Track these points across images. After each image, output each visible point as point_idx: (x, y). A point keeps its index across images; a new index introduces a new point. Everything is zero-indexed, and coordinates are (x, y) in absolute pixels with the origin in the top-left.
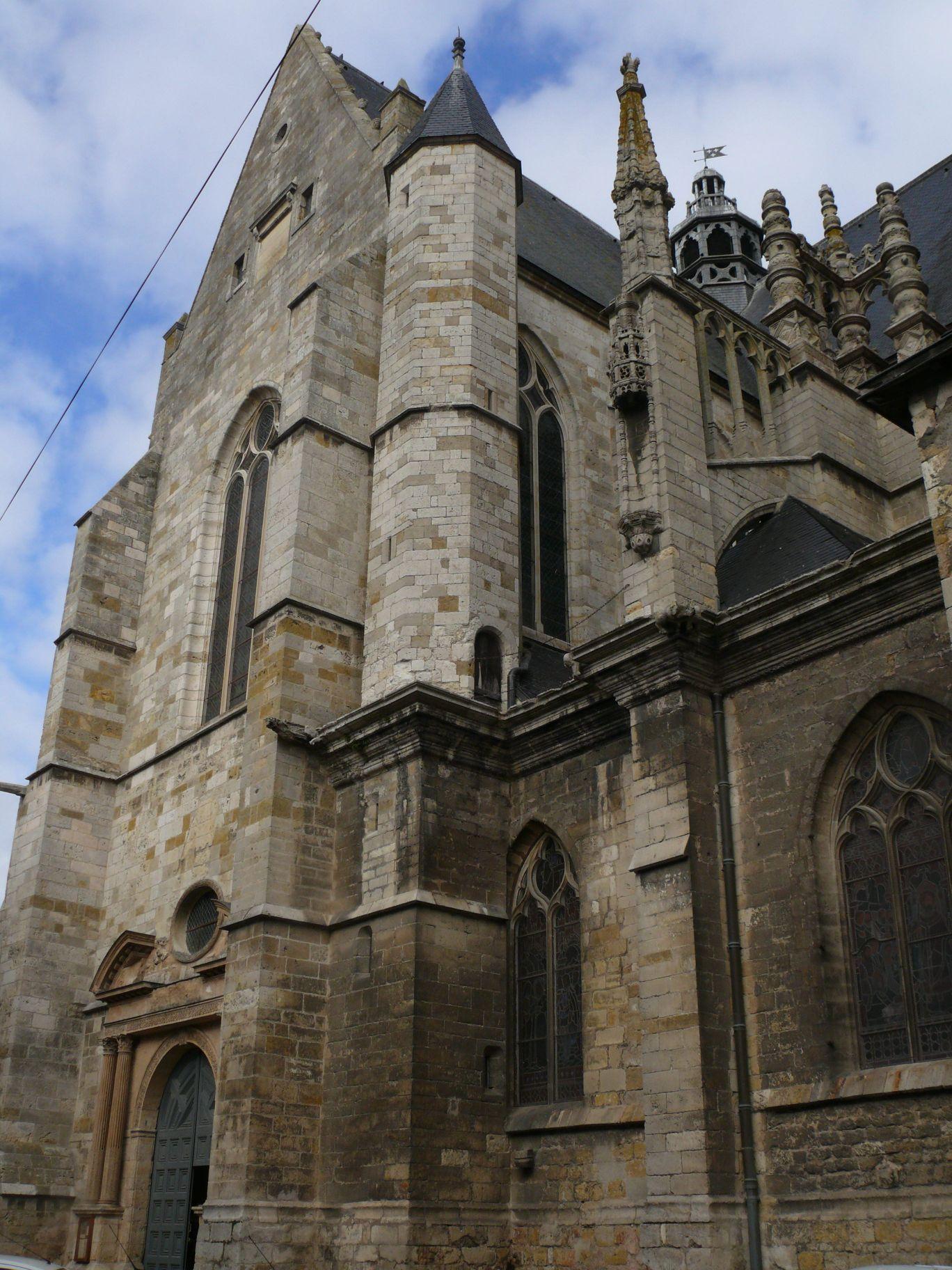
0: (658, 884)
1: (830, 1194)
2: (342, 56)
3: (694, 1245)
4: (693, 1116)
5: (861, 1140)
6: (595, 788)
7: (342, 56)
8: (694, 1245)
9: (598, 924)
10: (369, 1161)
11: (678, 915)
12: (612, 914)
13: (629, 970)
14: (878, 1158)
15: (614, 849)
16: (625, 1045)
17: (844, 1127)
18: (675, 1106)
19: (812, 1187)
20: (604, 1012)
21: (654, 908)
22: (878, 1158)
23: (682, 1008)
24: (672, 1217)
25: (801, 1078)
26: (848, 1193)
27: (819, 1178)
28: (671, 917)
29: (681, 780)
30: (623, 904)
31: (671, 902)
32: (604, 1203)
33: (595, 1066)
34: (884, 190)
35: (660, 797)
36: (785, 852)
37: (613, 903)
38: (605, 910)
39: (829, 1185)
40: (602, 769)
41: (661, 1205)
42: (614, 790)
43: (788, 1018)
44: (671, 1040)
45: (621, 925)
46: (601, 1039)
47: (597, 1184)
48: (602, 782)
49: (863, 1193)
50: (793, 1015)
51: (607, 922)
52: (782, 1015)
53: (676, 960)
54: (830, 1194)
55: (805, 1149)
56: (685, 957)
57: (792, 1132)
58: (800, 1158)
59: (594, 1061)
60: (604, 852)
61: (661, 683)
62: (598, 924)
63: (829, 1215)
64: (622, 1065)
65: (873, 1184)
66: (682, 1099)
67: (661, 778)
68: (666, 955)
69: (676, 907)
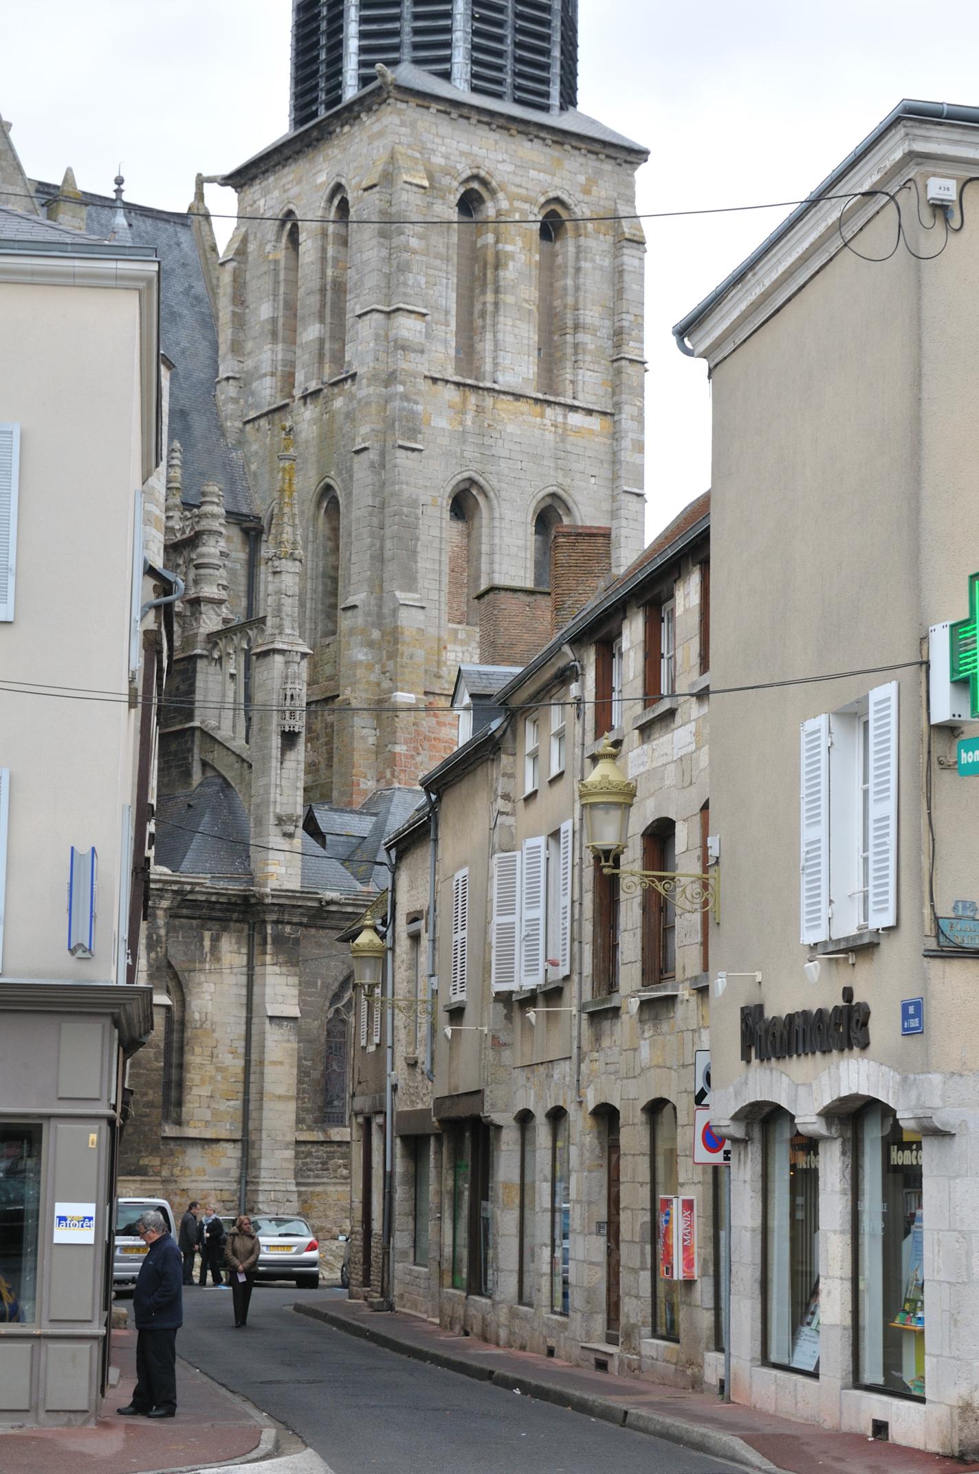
0: (281, 1026)
1: (317, 1180)
2: (69, 177)
3: (288, 1201)
4: (289, 1143)
5: (334, 1158)
6: (202, 945)
7: (69, 177)
8: (288, 1201)
9: (198, 1026)
10: (127, 1153)
11: (289, 1045)
12: (208, 1023)
13: (217, 1057)
14: (339, 1167)
15: (212, 986)
16: (212, 1097)
17: (327, 1152)
18: (280, 1138)
19: (309, 1177)
20: (199, 1077)
21: (276, 1038)
22: (339, 1167)
23: (288, 1091)
24: (277, 1188)
25: (310, 1129)
26: (325, 1180)
27: (312, 1173)
28: (285, 1045)
29: (296, 975)
30: (216, 1019)
31: (286, 1038)
32: (193, 1178)
33: (191, 1105)
34: (10, 125)
35: (283, 980)
36: (314, 1020)
37: (209, 1017)
38: (204, 1019)
39: (317, 1176)
40: (207, 935)
41: (270, 1183)
42: (215, 948)
43: (306, 1100)
44: (280, 1106)
45: (214, 1031)
46: (195, 1091)
47: (189, 1168)
48: (207, 943)
49: (333, 1181)
50: (309, 1099)
51: (204, 1026)
52: (304, 1098)
53: (287, 1067)
54: (317, 1180)
55: (308, 1160)
56: (291, 1067)
57: (303, 1152)
58: (305, 1164)
59: (190, 1102)
60: (205, 985)
61: (295, 920)
62: (198, 1026)
63: (319, 1189)
64: (209, 1107)
65: (336, 1177)
66: (284, 1135)
67: (284, 969)
68: (281, 1063)
69: (288, 1041)
